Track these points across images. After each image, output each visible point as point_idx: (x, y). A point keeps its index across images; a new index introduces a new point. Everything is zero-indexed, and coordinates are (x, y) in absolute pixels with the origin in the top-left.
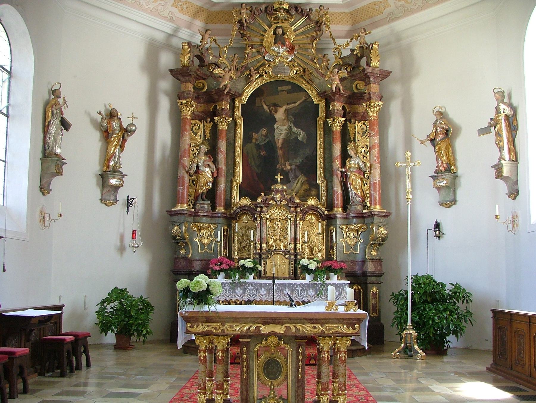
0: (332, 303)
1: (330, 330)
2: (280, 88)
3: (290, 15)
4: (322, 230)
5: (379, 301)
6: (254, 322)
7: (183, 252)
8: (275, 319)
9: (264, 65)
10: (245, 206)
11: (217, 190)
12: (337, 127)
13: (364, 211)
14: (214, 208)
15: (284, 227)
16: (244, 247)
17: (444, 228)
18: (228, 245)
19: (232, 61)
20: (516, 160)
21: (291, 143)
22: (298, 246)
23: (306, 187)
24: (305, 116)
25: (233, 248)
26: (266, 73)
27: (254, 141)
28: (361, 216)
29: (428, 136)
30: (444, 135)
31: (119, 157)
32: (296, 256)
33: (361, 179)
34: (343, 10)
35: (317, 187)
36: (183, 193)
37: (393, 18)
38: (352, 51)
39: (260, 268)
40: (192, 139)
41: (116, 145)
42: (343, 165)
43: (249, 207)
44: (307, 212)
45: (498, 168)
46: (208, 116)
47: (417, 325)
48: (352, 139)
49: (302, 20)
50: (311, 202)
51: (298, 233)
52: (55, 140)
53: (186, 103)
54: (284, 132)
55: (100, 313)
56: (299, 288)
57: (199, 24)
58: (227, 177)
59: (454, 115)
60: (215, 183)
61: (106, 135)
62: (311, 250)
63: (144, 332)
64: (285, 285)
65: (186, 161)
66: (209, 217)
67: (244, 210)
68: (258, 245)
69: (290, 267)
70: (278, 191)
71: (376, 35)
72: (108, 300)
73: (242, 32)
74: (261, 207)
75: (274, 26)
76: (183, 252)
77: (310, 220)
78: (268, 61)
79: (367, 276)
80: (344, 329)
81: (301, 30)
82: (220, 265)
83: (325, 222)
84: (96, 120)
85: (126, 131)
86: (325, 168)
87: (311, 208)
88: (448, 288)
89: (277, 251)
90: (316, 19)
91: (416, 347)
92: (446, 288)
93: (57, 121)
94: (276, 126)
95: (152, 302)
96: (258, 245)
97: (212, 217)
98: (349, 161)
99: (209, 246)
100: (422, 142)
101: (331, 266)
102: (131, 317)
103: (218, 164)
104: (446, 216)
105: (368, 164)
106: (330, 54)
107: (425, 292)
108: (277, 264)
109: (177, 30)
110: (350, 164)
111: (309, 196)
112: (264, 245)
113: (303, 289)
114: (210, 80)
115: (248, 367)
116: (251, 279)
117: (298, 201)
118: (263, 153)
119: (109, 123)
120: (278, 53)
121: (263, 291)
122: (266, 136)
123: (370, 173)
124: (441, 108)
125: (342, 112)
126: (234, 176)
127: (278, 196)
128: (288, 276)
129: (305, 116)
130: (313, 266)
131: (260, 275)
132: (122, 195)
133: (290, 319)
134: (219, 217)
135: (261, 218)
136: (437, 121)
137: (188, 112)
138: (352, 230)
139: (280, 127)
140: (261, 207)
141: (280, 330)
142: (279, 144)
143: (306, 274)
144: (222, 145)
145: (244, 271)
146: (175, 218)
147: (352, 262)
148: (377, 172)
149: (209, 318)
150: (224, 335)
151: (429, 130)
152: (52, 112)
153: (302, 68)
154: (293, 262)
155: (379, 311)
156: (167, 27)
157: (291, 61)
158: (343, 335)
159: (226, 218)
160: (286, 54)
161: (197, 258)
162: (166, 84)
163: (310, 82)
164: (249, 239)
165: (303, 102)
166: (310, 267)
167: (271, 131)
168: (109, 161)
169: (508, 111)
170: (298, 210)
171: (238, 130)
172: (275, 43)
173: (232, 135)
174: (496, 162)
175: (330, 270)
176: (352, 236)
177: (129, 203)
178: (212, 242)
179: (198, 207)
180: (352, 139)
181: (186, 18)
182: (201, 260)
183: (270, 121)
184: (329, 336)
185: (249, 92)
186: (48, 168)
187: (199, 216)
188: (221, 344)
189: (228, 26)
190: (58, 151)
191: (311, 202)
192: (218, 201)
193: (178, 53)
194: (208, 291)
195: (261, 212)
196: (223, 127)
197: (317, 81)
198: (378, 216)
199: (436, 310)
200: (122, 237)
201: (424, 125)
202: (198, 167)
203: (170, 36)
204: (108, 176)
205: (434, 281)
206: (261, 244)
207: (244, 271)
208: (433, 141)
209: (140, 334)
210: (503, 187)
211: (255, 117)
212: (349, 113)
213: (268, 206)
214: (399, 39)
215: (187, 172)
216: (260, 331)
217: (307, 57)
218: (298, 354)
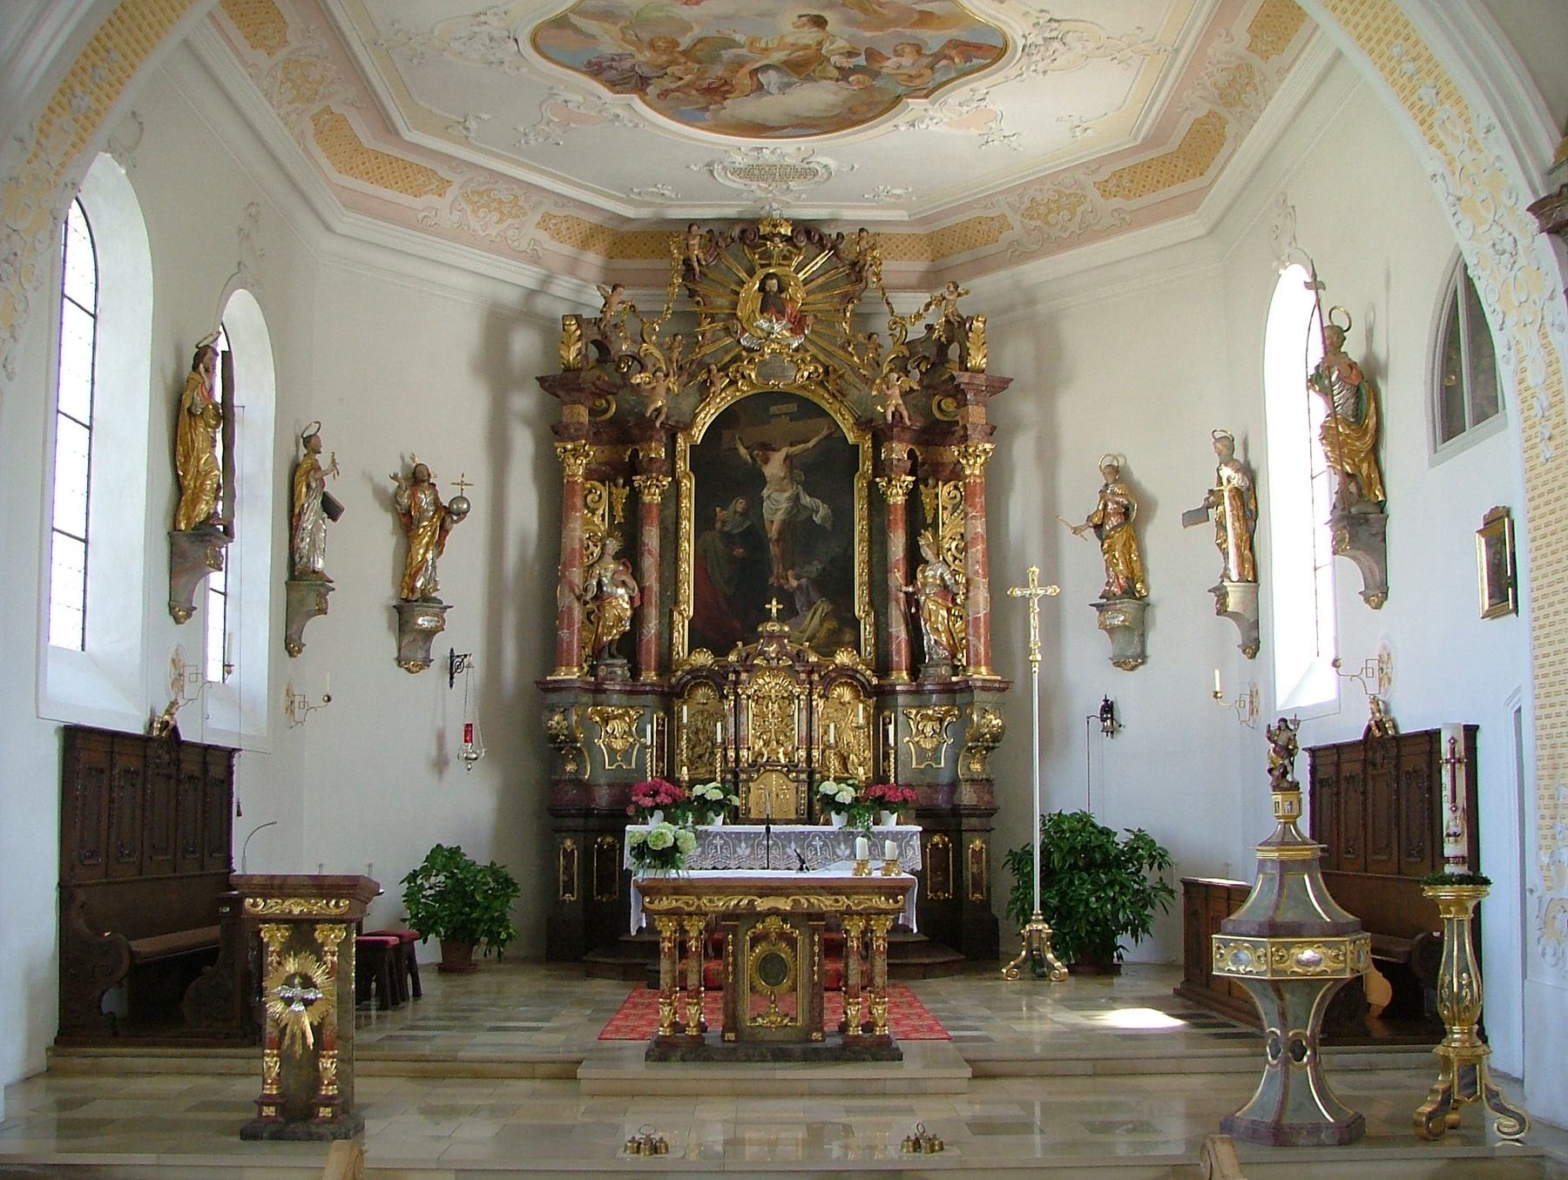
0: (862, 864)
1: (860, 903)
2: (774, 409)
3: (796, 247)
4: (867, 718)
5: (988, 868)
6: (746, 894)
7: (570, 768)
8: (778, 888)
9: (737, 358)
10: (703, 667)
11: (641, 634)
12: (897, 498)
13: (954, 679)
14: (635, 672)
15: (783, 713)
16: (700, 757)
17: (1124, 713)
18: (667, 749)
19: (670, 348)
20: (1255, 580)
21: (798, 527)
22: (815, 753)
23: (831, 625)
24: (830, 468)
25: (678, 758)
26: (743, 376)
27: (718, 525)
29: (1089, 518)
30: (1123, 516)
31: (434, 568)
32: (811, 774)
33: (949, 611)
34: (906, 231)
35: (855, 623)
36: (570, 643)
37: (1020, 254)
38: (930, 328)
39: (736, 801)
40: (588, 522)
41: (428, 544)
42: (911, 578)
43: (710, 669)
44: (834, 679)
45: (1221, 593)
46: (618, 473)
47: (1048, 913)
48: (929, 521)
49: (820, 260)
50: (843, 658)
51: (815, 727)
52: (313, 543)
53: (574, 449)
54: (785, 505)
55: (410, 897)
56: (818, 843)
57: (593, 260)
58: (662, 605)
59: (1144, 473)
60: (638, 617)
61: (407, 522)
62: (844, 760)
63: (503, 936)
64: (788, 836)
65: (576, 575)
66: (625, 692)
67: (699, 677)
68: (731, 754)
69: (798, 798)
70: (771, 637)
71: (983, 290)
72: (426, 872)
73: (691, 286)
74: (737, 673)
76: (570, 768)
77: (840, 696)
79: (961, 815)
80: (881, 902)
81: (821, 279)
82: (653, 796)
83: (871, 702)
84: (385, 490)
85: (448, 511)
87: (842, 670)
88: (1122, 838)
89: (772, 764)
90: (852, 257)
91: (1050, 956)
92: (1116, 839)
93: (317, 503)
94: (765, 493)
95: (514, 874)
96: (731, 754)
97: (631, 693)
98: (923, 572)
99: (626, 754)
100: (1076, 531)
101: (882, 797)
103: (642, 577)
104: (1125, 688)
105: (961, 579)
106: (881, 325)
107: (1072, 849)
108: (773, 792)
109: (546, 281)
110: (925, 577)
111: (840, 644)
112: (744, 753)
113: (825, 844)
114: (625, 394)
115: (735, 965)
116: (717, 824)
117: (813, 659)
119: (413, 496)
120: (769, 333)
121: (744, 849)
122: (744, 514)
123: (967, 598)
124: (1115, 457)
125: (909, 464)
126: (676, 602)
127: (772, 649)
128: (793, 817)
129: (830, 468)
130: (846, 795)
131: (735, 817)
132: (440, 648)
133: (800, 888)
134: (647, 693)
135: (737, 695)
136: (1107, 485)
137: (577, 469)
138: (930, 718)
139: (774, 495)
140: (737, 673)
141: (785, 904)
143: (833, 814)
144: (652, 537)
145: (704, 808)
146: (554, 698)
147: (929, 786)
148: (981, 596)
149: (678, 889)
150: (701, 913)
151: (1094, 505)
152: (308, 486)
153: (823, 365)
154: (804, 788)
155: (989, 889)
156: (527, 276)
157: (797, 350)
158: (881, 912)
159: (662, 694)
160: (787, 334)
161: (602, 781)
162: (525, 401)
163: (840, 395)
164: (714, 744)
165: (826, 438)
166: (839, 798)
168: (414, 578)
169: (1238, 480)
170: (816, 677)
171: (685, 503)
172: (762, 312)
173: (670, 512)
174: (1217, 584)
175: (882, 803)
176: (928, 730)
177: (454, 665)
178: (632, 745)
180: (929, 521)
181: (567, 249)
182: (610, 785)
184: (859, 914)
185: (706, 419)
186: (301, 602)
187: (605, 691)
188: (695, 927)
189: (663, 264)
190: (320, 564)
191: (843, 658)
192: (643, 659)
193: (553, 334)
194: (675, 848)
195: (737, 683)
196: (652, 497)
197: (853, 394)
198: (983, 689)
199: (1092, 883)
200: (441, 738)
201: (1081, 495)
202: (600, 585)
203: (531, 293)
204: (411, 607)
205: (1093, 825)
206: (737, 750)
207: (704, 808)
208: (1098, 528)
209: (494, 939)
210: (1235, 634)
211: (723, 472)
212: (923, 464)
213: (750, 669)
214: (1031, 301)
215: (578, 598)
216: (754, 907)
218: (812, 943)
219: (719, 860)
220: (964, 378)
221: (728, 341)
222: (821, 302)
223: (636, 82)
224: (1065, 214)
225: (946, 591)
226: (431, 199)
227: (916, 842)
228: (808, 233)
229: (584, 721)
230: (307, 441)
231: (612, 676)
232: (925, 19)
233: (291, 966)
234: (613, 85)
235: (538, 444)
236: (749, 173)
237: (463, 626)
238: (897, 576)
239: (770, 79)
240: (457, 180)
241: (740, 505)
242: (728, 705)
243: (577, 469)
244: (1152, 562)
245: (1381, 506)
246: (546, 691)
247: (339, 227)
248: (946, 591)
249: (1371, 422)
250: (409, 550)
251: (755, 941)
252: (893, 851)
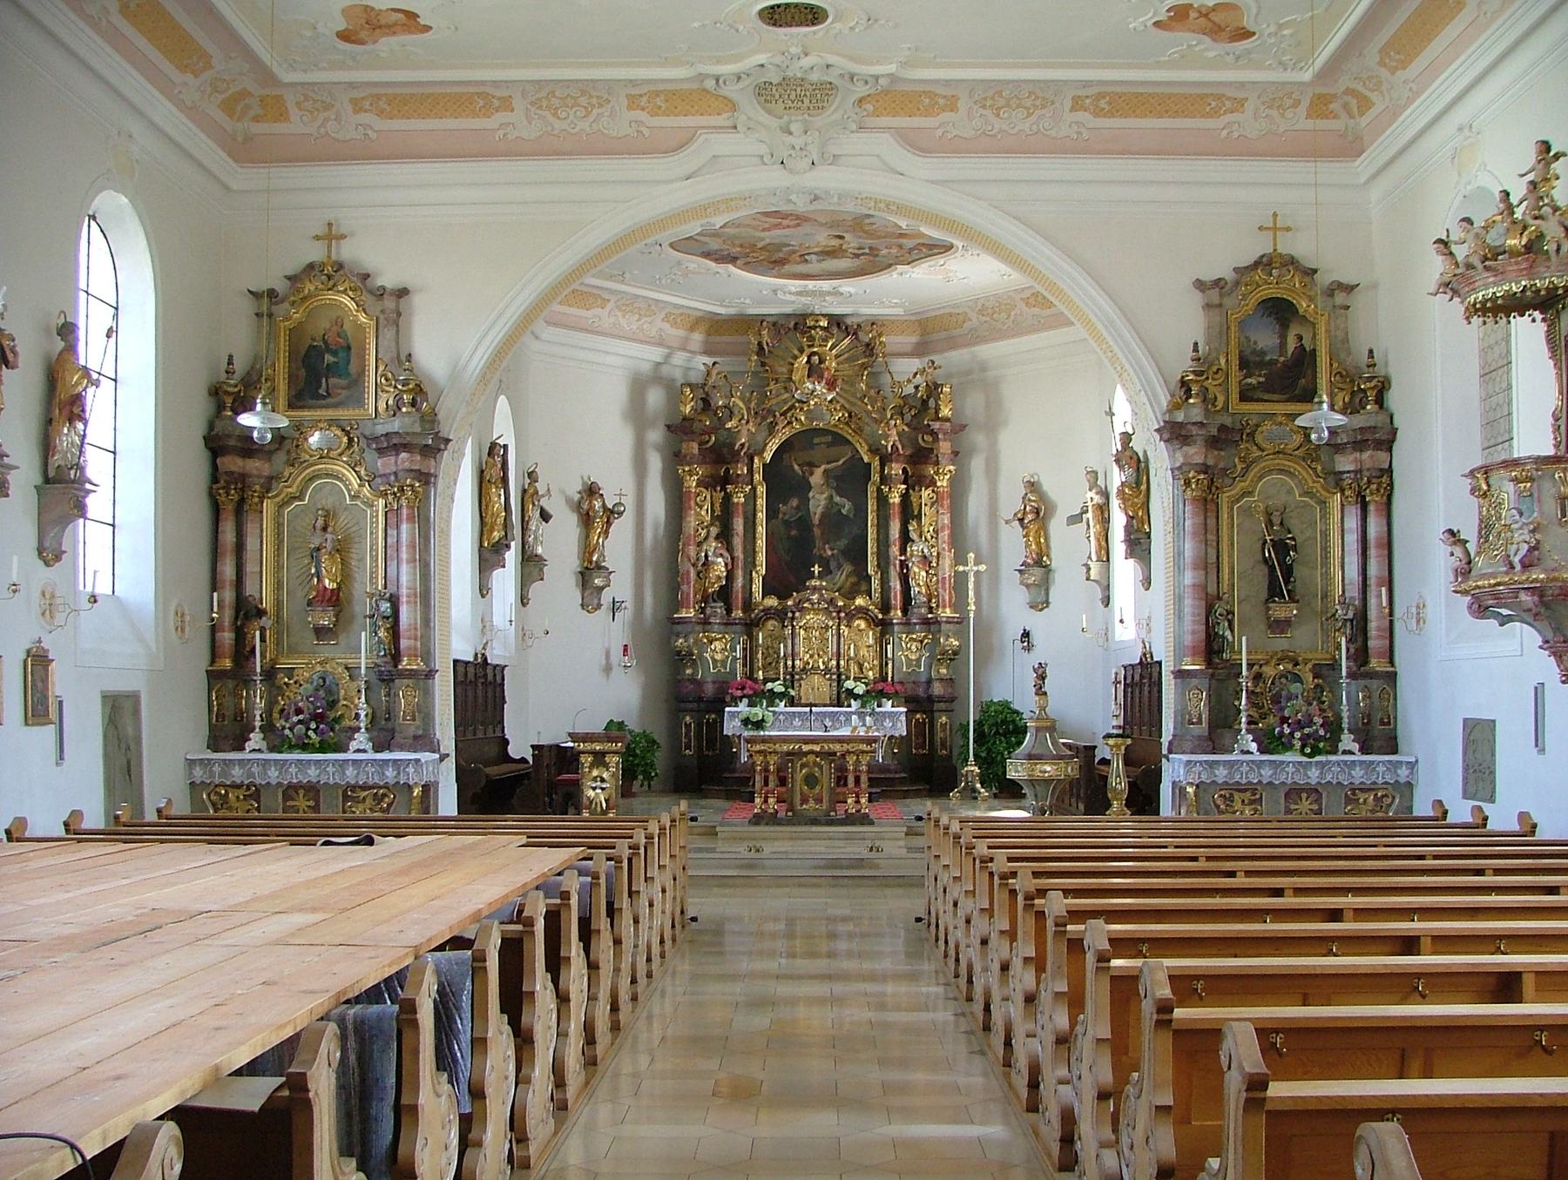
0: (855, 728)
2: (816, 441)
9: (792, 407)
12: (895, 499)
14: (729, 611)
15: (819, 636)
17: (1036, 638)
19: (750, 401)
21: (833, 519)
23: (853, 579)
24: (852, 479)
28: (926, 622)
32: (839, 676)
37: (976, 339)
38: (917, 387)
39: (793, 693)
42: (903, 551)
50: (859, 601)
57: (698, 337)
61: (587, 520)
62: (861, 667)
65: (692, 550)
67: (768, 613)
70: (815, 588)
75: (808, 351)
78: (799, 401)
80: (864, 747)
85: (612, 512)
86: (879, 554)
87: (860, 609)
99: (724, 663)
102: (635, 756)
108: (816, 687)
109: (668, 356)
116: (781, 706)
117: (841, 604)
118: (793, 533)
121: (797, 722)
122: (798, 508)
126: (755, 566)
127: (815, 597)
129: (852, 479)
130: (860, 689)
131: (792, 702)
137: (692, 482)
141: (817, 748)
142: (816, 520)
144: (739, 525)
145: (772, 697)
146: (679, 628)
148: (947, 562)
149: (765, 740)
150: (775, 752)
156: (656, 354)
162: (656, 435)
163: (859, 431)
167: (805, 501)
168: (591, 554)
169: (1098, 499)
171: (759, 502)
177: (615, 607)
179: (708, 611)
181: (681, 333)
183: (802, 488)
188: (773, 759)
190: (540, 550)
191: (859, 601)
193: (675, 393)
195: (793, 618)
196: (739, 499)
197: (867, 429)
201: (1011, 500)
204: (590, 573)
207: (772, 697)
208: (1021, 520)
213: (802, 610)
217: (854, 395)
219: (785, 725)
220: (936, 425)
221: (786, 395)
222: (847, 370)
223: (733, 260)
224: (1004, 315)
225: (925, 560)
226: (598, 311)
227: (903, 718)
228: (837, 321)
229: (697, 641)
230: (530, 475)
231: (715, 614)
233: (595, 773)
234: (716, 260)
235: (664, 461)
236: (799, 294)
237: (620, 586)
238: (895, 550)
240: (613, 298)
241: (795, 502)
242: (788, 631)
243: (692, 482)
244: (1053, 544)
245: (1148, 535)
246: (672, 624)
247: (544, 336)
248: (925, 560)
249: (1143, 487)
250: (587, 536)
251: (803, 766)
252: (893, 719)
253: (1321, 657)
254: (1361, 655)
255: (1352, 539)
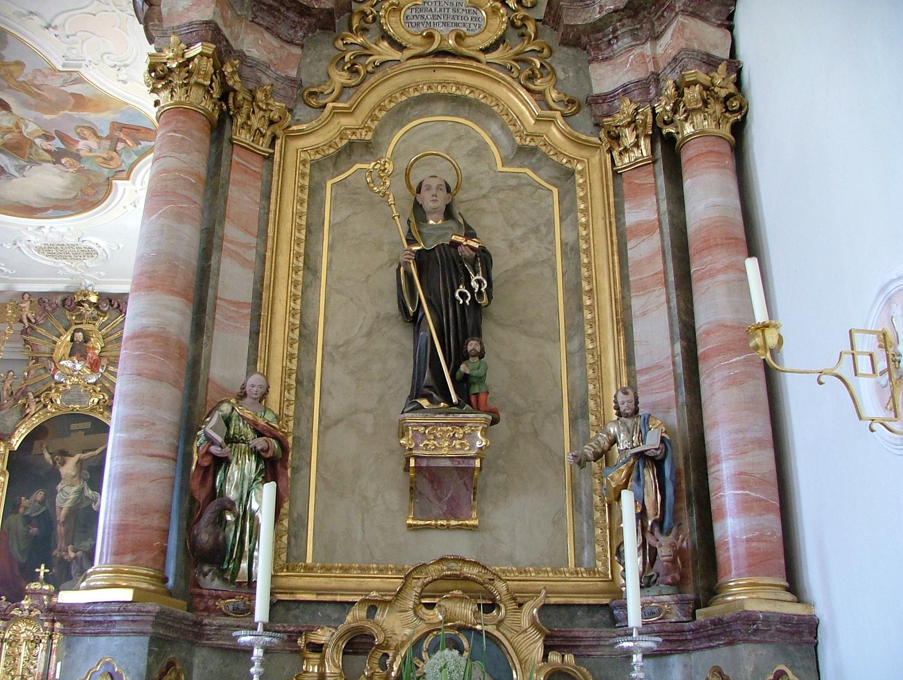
2: (74, 427)
122: (42, 503)
142: (61, 516)
167: (52, 494)
232: (80, 102)
239: (93, 299)
253: (575, 586)
254: (695, 569)
255: (648, 251)
